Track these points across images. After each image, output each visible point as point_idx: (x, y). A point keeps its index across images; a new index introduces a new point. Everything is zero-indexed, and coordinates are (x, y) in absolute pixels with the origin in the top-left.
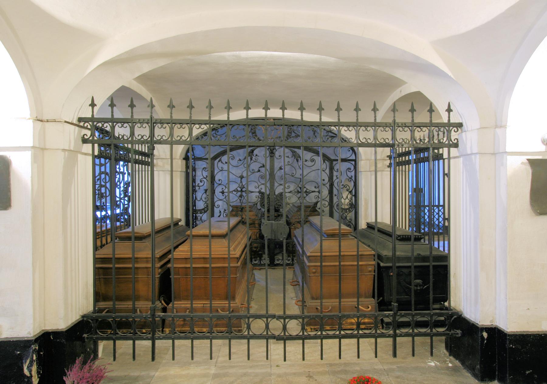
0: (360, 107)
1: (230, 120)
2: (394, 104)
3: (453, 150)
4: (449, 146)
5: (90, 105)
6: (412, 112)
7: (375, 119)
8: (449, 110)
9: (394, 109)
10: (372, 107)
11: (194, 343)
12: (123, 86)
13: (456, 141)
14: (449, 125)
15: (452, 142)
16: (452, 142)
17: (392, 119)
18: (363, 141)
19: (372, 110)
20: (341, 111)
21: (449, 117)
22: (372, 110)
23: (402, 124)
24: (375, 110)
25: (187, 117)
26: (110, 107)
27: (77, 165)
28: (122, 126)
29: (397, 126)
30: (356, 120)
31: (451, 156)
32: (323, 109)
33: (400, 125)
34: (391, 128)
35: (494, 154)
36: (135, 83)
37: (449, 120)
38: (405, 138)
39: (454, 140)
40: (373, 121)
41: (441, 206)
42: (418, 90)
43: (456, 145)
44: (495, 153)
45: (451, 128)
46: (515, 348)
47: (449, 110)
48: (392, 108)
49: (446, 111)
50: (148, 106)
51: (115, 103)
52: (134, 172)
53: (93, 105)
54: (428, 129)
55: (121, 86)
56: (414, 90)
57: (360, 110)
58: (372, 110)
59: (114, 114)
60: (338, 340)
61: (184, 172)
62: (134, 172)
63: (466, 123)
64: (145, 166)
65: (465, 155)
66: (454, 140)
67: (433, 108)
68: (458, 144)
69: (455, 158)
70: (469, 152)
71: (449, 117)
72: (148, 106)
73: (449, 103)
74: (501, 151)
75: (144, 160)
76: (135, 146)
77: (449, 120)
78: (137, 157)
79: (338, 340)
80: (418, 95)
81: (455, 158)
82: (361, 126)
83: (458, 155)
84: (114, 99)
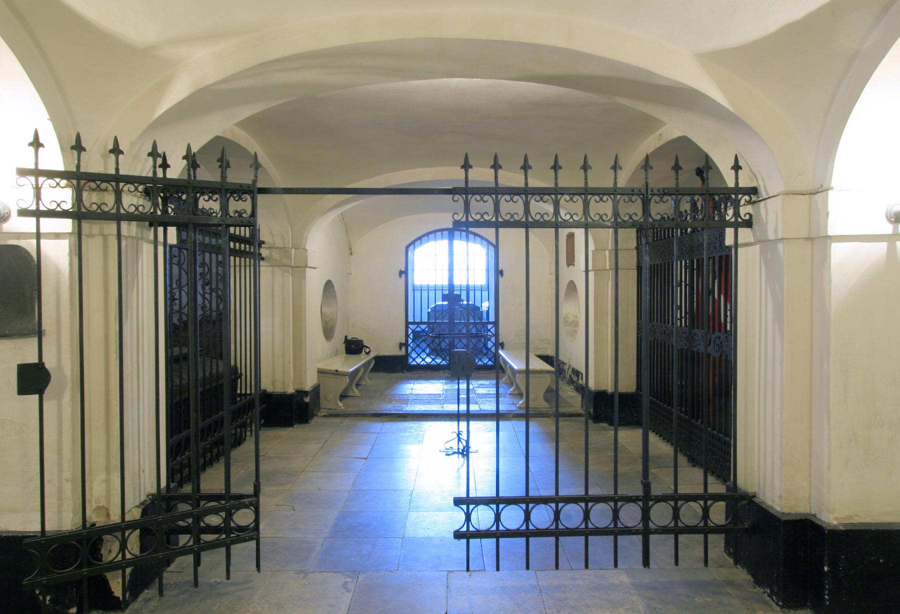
0: (530, 164)
1: (740, 186)
2: (647, 156)
3: (744, 233)
4: (736, 226)
5: (732, 168)
6: (646, 171)
7: (615, 183)
8: (737, 167)
9: (646, 165)
10: (522, 164)
11: (619, 542)
12: (685, 136)
13: (747, 217)
14: (738, 190)
15: (741, 218)
16: (741, 218)
17: (644, 182)
18: (565, 218)
19: (581, 168)
20: (530, 170)
21: (737, 179)
22: (611, 168)
23: (659, 191)
24: (615, 167)
25: (551, 185)
26: (733, 171)
27: (142, 255)
28: (210, 198)
29: (651, 194)
30: (584, 184)
31: (739, 242)
32: (530, 168)
33: (655, 191)
34: (641, 196)
35: (809, 239)
36: (238, 130)
37: (737, 183)
38: (633, 212)
39: (745, 216)
40: (583, 186)
41: (491, 323)
42: (681, 134)
43: (748, 224)
44: (812, 237)
45: (740, 196)
46: (829, 566)
47: (737, 167)
48: (644, 163)
49: (551, 168)
50: (251, 166)
51: (500, 163)
52: (258, 267)
53: (677, 168)
54: (582, 198)
55: (214, 136)
56: (677, 134)
57: (530, 168)
58: (581, 168)
59: (588, 180)
60: (524, 539)
61: (584, 271)
62: (258, 267)
63: (765, 187)
64: (240, 258)
65: (763, 241)
66: (745, 216)
67: (710, 164)
68: (752, 223)
69: (747, 245)
70: (771, 236)
71: (737, 179)
72: (251, 166)
73: (736, 156)
74: (822, 234)
75: (247, 246)
76: (240, 231)
77: (737, 183)
78: (232, 244)
79: (524, 539)
80: (684, 142)
81: (747, 245)
82: (563, 194)
83: (752, 240)
84: (650, 159)
